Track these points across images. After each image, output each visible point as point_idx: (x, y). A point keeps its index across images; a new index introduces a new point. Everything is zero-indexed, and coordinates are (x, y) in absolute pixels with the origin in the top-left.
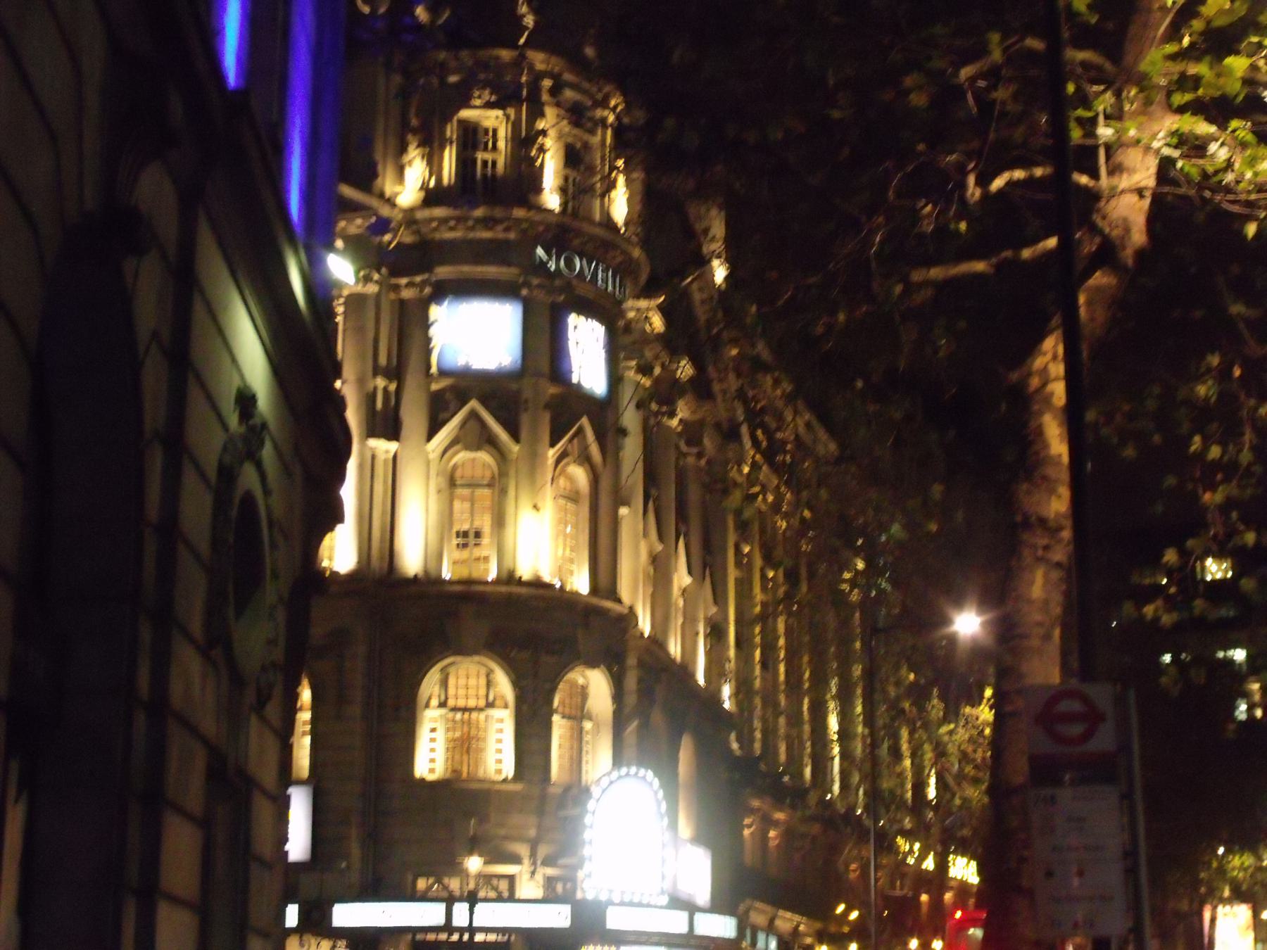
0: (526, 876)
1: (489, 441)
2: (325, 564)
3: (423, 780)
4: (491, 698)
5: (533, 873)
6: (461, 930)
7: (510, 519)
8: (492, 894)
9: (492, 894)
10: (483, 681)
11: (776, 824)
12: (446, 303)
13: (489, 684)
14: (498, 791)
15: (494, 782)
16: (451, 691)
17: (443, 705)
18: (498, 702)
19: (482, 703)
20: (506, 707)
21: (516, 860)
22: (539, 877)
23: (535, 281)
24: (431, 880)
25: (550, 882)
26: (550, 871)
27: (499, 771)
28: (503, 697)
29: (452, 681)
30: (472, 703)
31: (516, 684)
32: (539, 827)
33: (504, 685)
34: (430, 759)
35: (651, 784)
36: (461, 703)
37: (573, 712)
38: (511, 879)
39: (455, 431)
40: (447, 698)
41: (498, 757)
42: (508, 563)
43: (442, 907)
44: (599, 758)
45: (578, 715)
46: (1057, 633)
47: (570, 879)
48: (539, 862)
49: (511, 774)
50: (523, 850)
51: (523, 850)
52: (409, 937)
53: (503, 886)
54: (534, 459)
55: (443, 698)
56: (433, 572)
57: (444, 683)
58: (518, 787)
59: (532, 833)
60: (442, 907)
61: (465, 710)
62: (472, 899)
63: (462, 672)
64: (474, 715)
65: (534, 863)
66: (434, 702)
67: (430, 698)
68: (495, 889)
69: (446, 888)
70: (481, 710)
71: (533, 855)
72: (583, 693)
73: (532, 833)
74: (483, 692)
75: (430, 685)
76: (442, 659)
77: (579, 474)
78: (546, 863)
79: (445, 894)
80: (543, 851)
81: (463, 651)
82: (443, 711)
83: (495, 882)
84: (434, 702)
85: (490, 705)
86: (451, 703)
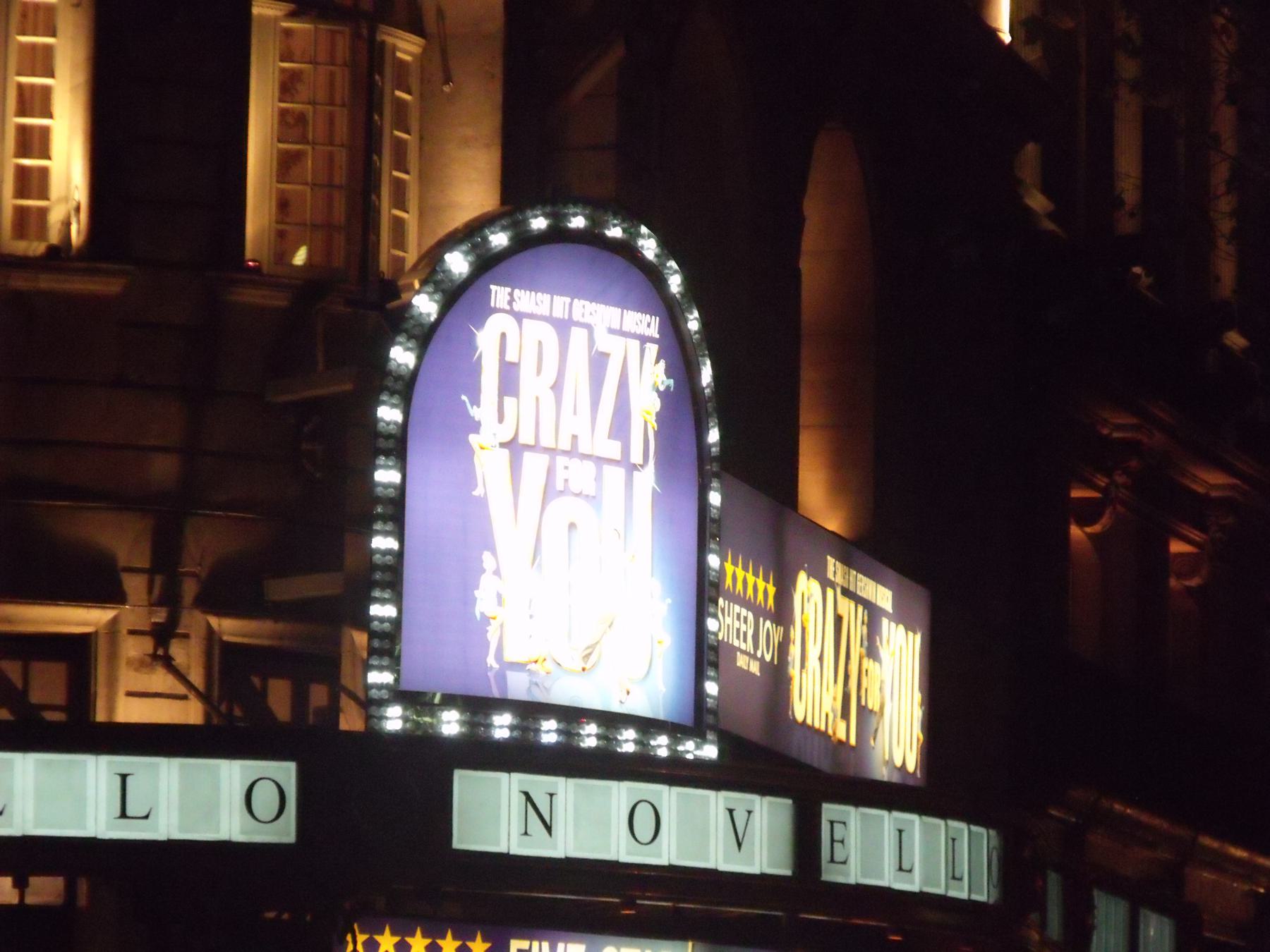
0: (134, 648)
5: (163, 635)
11: (1197, 510)
12: (474, 412)
21: (105, 591)
22: (187, 654)
25: (232, 671)
26: (229, 628)
35: (654, 274)
38: (75, 652)
47: (319, 664)
48: (189, 589)
49: (77, 233)
50: (125, 541)
51: (125, 541)
58: (107, 286)
65: (169, 599)
71: (165, 563)
78: (216, 599)
80: (206, 542)
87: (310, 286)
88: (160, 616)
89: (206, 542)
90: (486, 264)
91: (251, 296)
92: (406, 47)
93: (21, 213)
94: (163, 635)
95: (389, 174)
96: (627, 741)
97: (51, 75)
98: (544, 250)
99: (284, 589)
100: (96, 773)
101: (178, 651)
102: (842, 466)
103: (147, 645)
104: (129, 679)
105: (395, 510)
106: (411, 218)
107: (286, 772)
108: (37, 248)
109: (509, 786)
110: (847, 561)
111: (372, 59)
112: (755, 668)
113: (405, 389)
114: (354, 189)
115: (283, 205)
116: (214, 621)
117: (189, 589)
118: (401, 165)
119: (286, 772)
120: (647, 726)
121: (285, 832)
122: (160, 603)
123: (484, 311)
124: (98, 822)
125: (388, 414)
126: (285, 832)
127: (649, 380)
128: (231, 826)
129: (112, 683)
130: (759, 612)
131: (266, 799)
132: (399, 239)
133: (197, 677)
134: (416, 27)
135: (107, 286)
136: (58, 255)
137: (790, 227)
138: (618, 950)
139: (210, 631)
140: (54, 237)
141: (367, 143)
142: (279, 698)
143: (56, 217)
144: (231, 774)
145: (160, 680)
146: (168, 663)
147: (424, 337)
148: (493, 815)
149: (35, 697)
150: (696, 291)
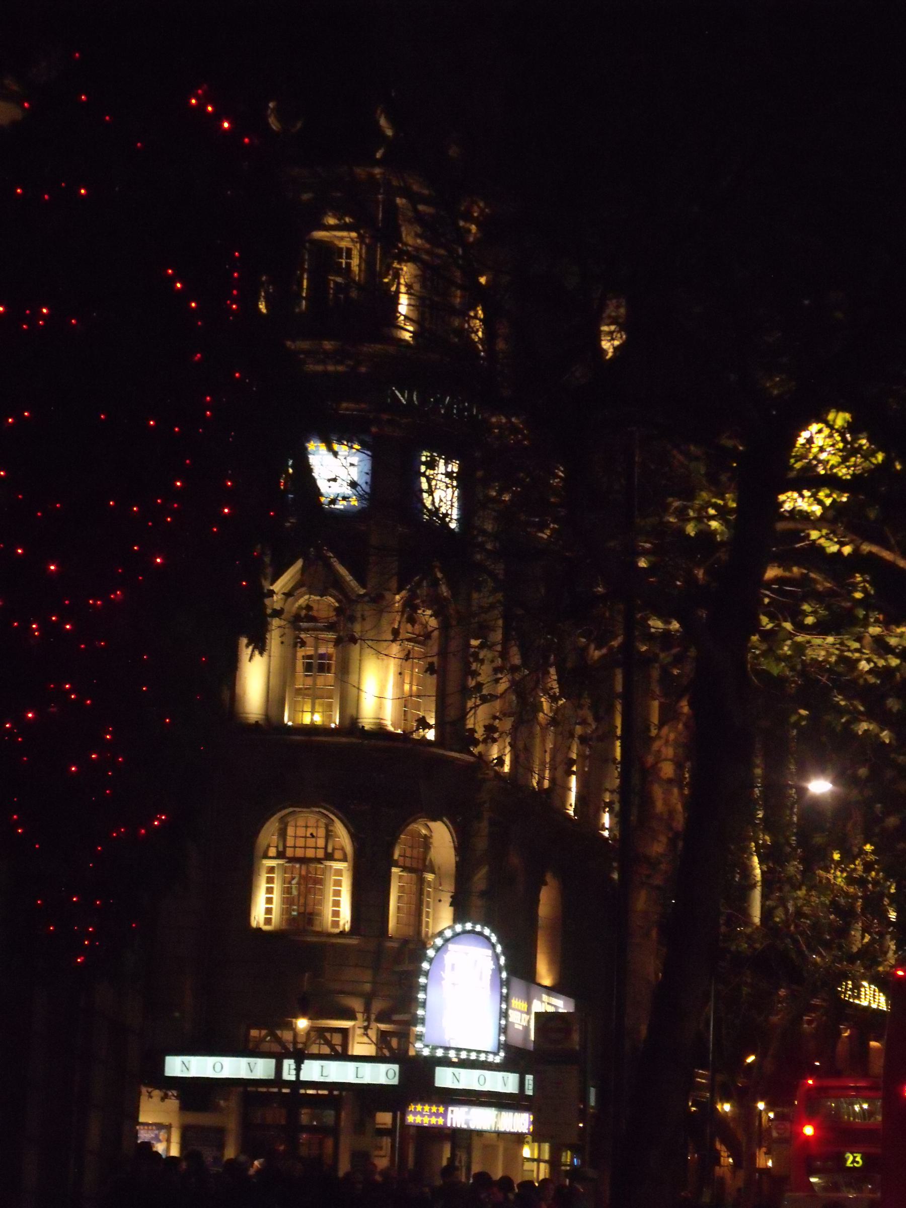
0: (359, 1031)
1: (334, 584)
2: (532, 1117)
3: (259, 930)
4: (330, 850)
5: (366, 1028)
6: (288, 1083)
7: (354, 666)
8: (326, 1050)
9: (326, 1050)
10: (322, 832)
12: (443, 975)
13: (329, 835)
14: (333, 945)
15: (330, 935)
16: (290, 842)
17: (280, 855)
18: (338, 854)
19: (320, 854)
20: (344, 860)
21: (350, 1015)
22: (372, 1033)
23: (385, 417)
24: (264, 1032)
25: (383, 1038)
26: (383, 1027)
27: (336, 924)
28: (343, 849)
29: (290, 831)
30: (310, 853)
31: (353, 837)
32: (374, 983)
33: (343, 837)
34: (265, 907)
35: (493, 946)
36: (299, 853)
37: (415, 865)
38: (344, 1032)
39: (298, 577)
40: (285, 847)
41: (338, 908)
42: (351, 711)
43: (272, 1062)
44: (442, 918)
45: (420, 866)
46: (654, 934)
47: (405, 1035)
48: (373, 1017)
49: (347, 928)
50: (357, 1004)
51: (357, 1004)
52: (241, 1089)
53: (337, 1039)
54: (378, 599)
55: (281, 849)
56: (273, 713)
57: (283, 834)
58: (353, 941)
59: (367, 987)
60: (272, 1062)
61: (303, 861)
62: (300, 1057)
63: (301, 822)
64: (313, 866)
65: (368, 1019)
66: (272, 852)
67: (269, 846)
68: (328, 1043)
69: (278, 1040)
70: (319, 861)
71: (367, 1010)
72: (426, 843)
73: (367, 987)
74: (321, 842)
75: (269, 836)
76: (280, 810)
77: (428, 618)
78: (379, 1020)
79: (276, 1048)
80: (378, 1005)
81: (305, 801)
82: (281, 862)
83: (328, 1035)
84: (272, 852)
85: (329, 857)
86: (289, 853)
87: (405, 942)
88: (366, 1024)
89: (378, 1005)
90: (447, 941)
91: (390, 944)
92: (430, 877)
93: (333, 921)
94: (366, 1028)
95: (425, 909)
96: (482, 1057)
97: (341, 876)
98: (462, 936)
99: (396, 1017)
100: (351, 1066)
101: (370, 1032)
102: (552, 962)
103: (362, 1031)
104: (358, 1039)
105: (424, 1005)
106: (430, 920)
107: (396, 1067)
108: (337, 931)
109: (449, 1071)
110: (549, 995)
111: (421, 881)
112: (521, 1028)
113: (427, 974)
114: (416, 911)
115: (399, 908)
116: (379, 1025)
117: (373, 1017)
118: (428, 917)
119: (396, 1067)
120: (487, 1053)
121: (395, 1081)
122: (365, 1021)
123: (447, 950)
124: (351, 1079)
125: (422, 980)
126: (395, 1081)
127: (490, 965)
128: (382, 1080)
129: (353, 1037)
130: (522, 1012)
131: (391, 1074)
132: (427, 926)
133: (374, 1039)
134: (433, 873)
135: (353, 941)
136: (342, 934)
137: (537, 901)
138: (467, 1123)
139: (378, 1029)
140: (341, 929)
141: (420, 892)
142: (394, 1042)
143: (341, 923)
144: (383, 1067)
145: (365, 1039)
146: (367, 1035)
147: (431, 961)
148: (445, 1078)
149: (334, 1042)
150: (500, 941)
